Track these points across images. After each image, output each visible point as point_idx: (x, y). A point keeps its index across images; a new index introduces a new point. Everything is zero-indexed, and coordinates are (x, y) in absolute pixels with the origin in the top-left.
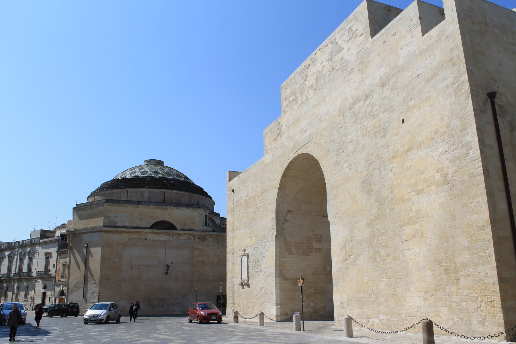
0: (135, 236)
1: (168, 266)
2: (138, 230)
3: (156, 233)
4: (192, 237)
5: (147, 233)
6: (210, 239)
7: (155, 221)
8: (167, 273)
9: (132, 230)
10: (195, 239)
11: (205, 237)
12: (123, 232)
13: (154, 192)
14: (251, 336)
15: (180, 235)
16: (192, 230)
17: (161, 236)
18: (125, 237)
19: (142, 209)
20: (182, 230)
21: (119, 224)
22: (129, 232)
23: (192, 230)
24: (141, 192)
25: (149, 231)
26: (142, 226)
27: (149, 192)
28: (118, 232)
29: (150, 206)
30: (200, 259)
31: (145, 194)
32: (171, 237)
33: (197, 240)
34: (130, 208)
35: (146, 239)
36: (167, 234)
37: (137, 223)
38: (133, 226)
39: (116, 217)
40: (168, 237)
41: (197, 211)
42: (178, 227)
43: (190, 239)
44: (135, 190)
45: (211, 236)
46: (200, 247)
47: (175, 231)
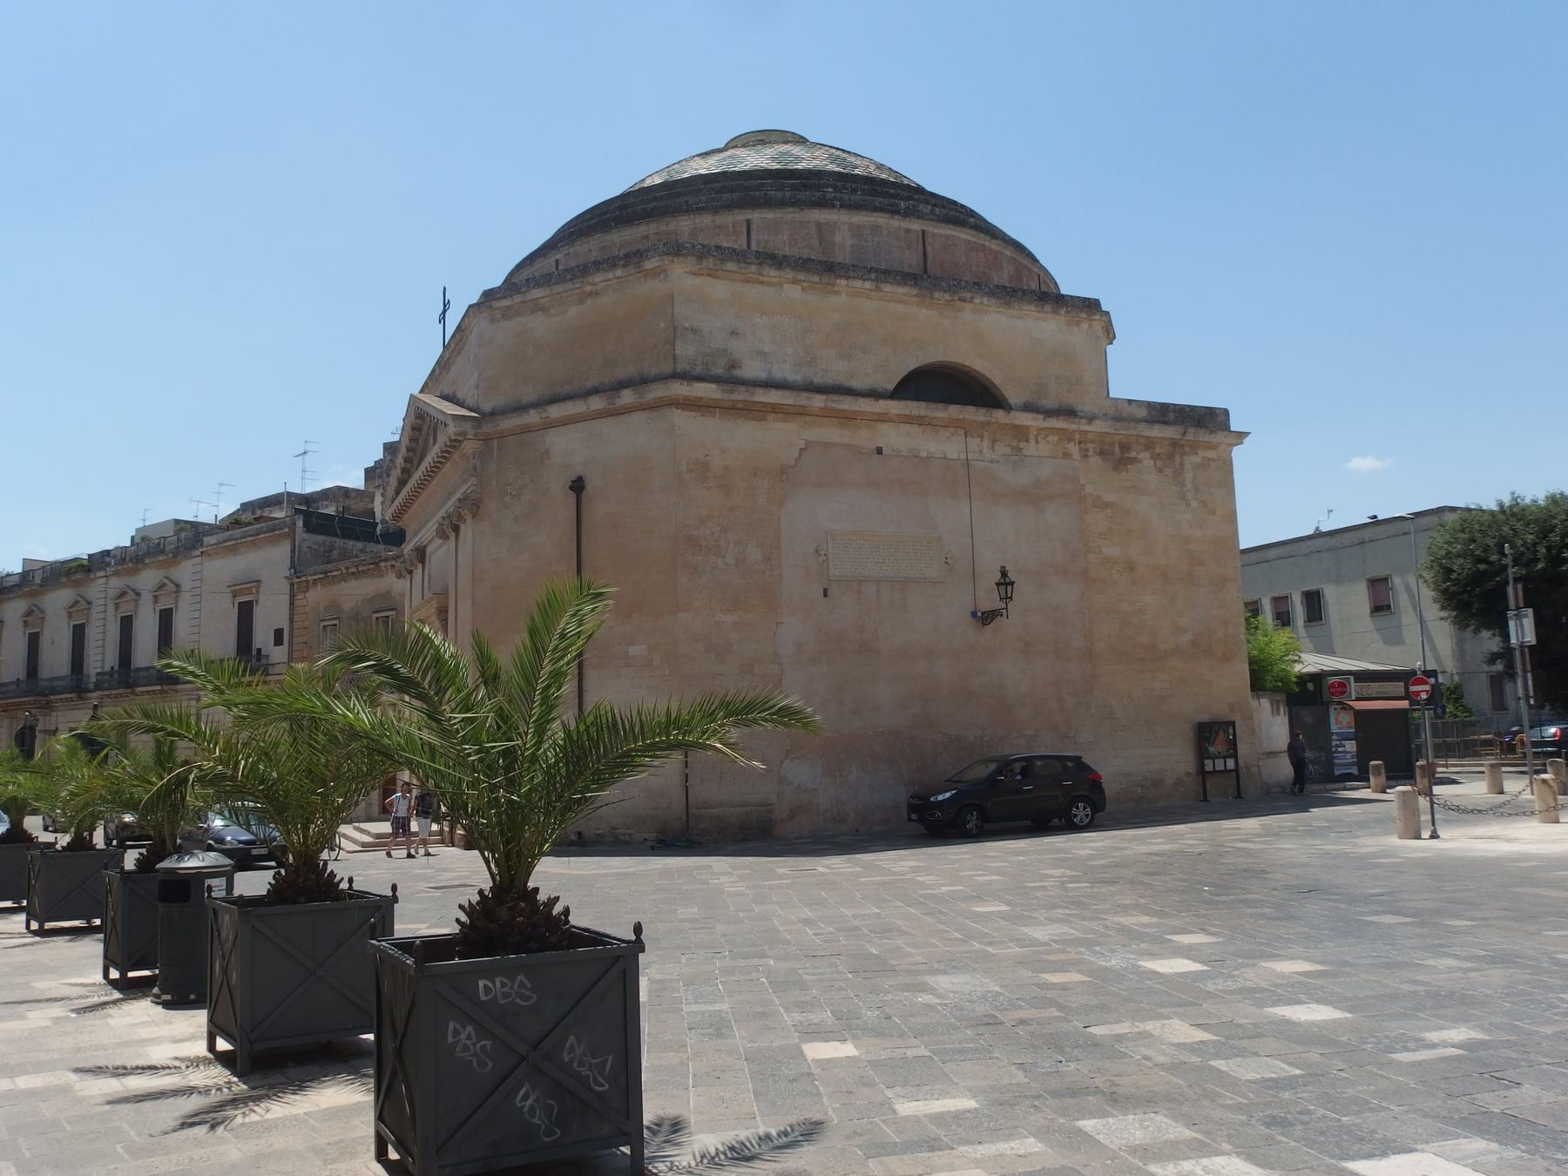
0: (831, 433)
1: (1005, 582)
2: (846, 404)
3: (921, 421)
4: (1073, 449)
5: (883, 418)
6: (1145, 456)
7: (911, 364)
8: (987, 618)
9: (818, 401)
10: (1085, 454)
11: (1125, 447)
12: (775, 409)
13: (876, 229)
14: (1364, 914)
15: (1021, 433)
16: (1070, 413)
17: (912, 435)
18: (778, 438)
19: (849, 301)
20: (1029, 408)
21: (752, 369)
22: (802, 412)
23: (1070, 413)
24: (819, 226)
25: (895, 407)
26: (855, 384)
27: (856, 230)
28: (847, 418)
29: (887, 288)
30: (1113, 551)
31: (838, 238)
32: (986, 444)
33: (1094, 460)
34: (794, 291)
35: (879, 451)
36: (967, 429)
37: (835, 369)
38: (818, 380)
39: (734, 333)
40: (974, 443)
41: (1085, 326)
42: (1013, 399)
43: (1067, 455)
44: (791, 215)
45: (1149, 444)
46: (1109, 497)
47: (1000, 415)
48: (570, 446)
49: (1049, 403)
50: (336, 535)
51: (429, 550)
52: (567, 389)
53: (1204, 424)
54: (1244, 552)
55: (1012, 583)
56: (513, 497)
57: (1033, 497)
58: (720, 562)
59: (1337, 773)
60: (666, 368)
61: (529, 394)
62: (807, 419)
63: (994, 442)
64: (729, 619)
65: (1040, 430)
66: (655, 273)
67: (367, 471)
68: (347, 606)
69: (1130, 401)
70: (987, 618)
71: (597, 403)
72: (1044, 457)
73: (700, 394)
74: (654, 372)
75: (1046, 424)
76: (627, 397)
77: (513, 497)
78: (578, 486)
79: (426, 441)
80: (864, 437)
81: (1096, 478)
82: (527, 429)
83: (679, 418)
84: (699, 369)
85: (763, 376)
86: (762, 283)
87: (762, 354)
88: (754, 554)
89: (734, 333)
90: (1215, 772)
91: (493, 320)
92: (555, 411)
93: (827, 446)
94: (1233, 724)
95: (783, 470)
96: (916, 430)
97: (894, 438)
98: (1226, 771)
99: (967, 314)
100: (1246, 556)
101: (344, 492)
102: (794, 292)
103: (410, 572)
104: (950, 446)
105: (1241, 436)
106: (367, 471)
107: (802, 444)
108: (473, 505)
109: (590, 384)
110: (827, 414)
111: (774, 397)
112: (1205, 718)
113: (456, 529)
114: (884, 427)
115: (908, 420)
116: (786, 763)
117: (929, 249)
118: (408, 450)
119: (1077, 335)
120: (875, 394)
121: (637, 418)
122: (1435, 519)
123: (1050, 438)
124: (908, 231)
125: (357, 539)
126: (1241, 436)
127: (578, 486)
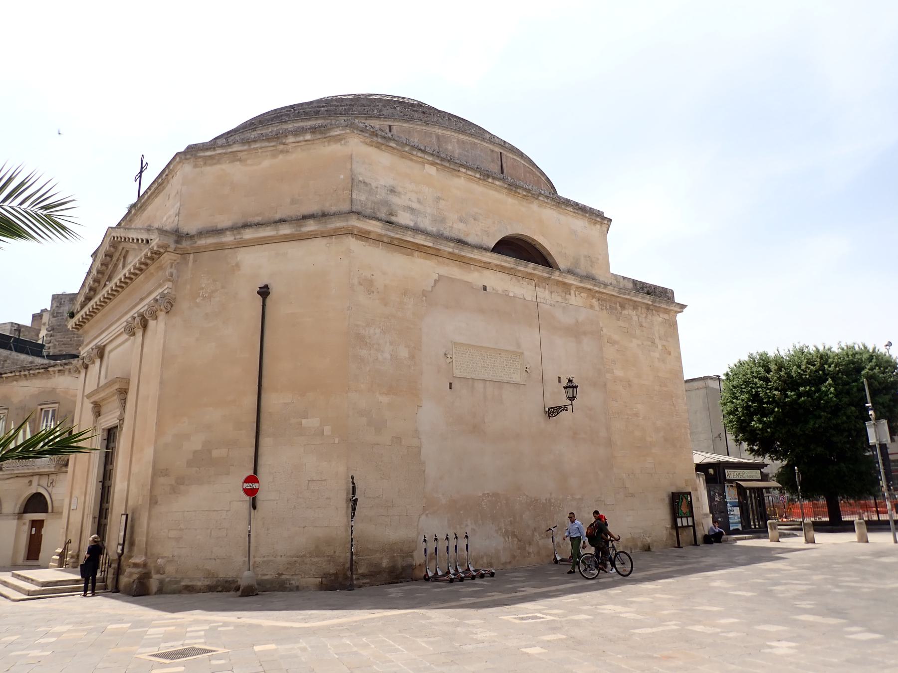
0: (454, 271)
3: (511, 272)
5: (487, 266)
8: (553, 412)
9: (448, 248)
12: (419, 248)
15: (566, 287)
18: (422, 270)
19: (461, 185)
20: (570, 272)
21: (404, 218)
27: (462, 143)
30: (619, 373)
35: (485, 288)
37: (458, 229)
43: (592, 307)
48: (257, 263)
49: (582, 271)
50: (10, 349)
51: (108, 349)
52: (258, 219)
53: (658, 298)
54: (687, 381)
55: (576, 387)
56: (204, 298)
57: (575, 332)
58: (380, 357)
59: (731, 528)
60: (345, 207)
61: (224, 221)
62: (441, 259)
63: (551, 293)
64: (384, 399)
65: (578, 288)
66: (338, 139)
67: (34, 316)
68: (16, 400)
69: (624, 278)
70: (553, 412)
71: (285, 230)
72: (577, 307)
73: (371, 228)
74: (334, 209)
75: (582, 285)
76: (311, 226)
77: (204, 298)
78: (264, 292)
79: (116, 265)
80: (477, 277)
81: (609, 325)
82: (221, 247)
83: (353, 243)
84: (368, 211)
85: (412, 224)
86: (411, 160)
87: (412, 210)
88: (404, 353)
89: (392, 191)
90: (683, 527)
91: (196, 166)
92: (248, 234)
93: (452, 280)
94: (690, 494)
95: (424, 293)
96: (507, 277)
97: (495, 281)
98: (688, 526)
99: (534, 206)
100: (688, 384)
101: (19, 328)
102: (431, 170)
103: (86, 367)
104: (522, 290)
105: (683, 307)
106: (34, 316)
107: (436, 277)
108: (168, 304)
109: (278, 216)
110: (454, 258)
111: (420, 240)
112: (674, 491)
113: (145, 326)
114: (487, 273)
115: (501, 269)
116: (423, 517)
117: (504, 165)
118: (98, 272)
119: (594, 231)
120: (486, 249)
121: (319, 244)
122: (701, 384)
123: (582, 294)
124: (492, 151)
125: (27, 353)
126: (683, 307)
127: (264, 292)
